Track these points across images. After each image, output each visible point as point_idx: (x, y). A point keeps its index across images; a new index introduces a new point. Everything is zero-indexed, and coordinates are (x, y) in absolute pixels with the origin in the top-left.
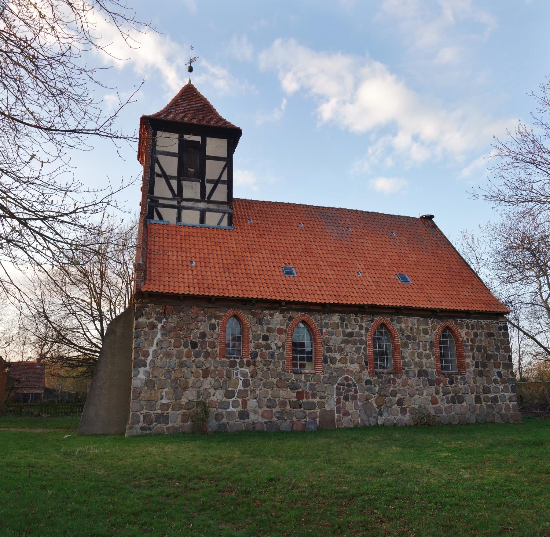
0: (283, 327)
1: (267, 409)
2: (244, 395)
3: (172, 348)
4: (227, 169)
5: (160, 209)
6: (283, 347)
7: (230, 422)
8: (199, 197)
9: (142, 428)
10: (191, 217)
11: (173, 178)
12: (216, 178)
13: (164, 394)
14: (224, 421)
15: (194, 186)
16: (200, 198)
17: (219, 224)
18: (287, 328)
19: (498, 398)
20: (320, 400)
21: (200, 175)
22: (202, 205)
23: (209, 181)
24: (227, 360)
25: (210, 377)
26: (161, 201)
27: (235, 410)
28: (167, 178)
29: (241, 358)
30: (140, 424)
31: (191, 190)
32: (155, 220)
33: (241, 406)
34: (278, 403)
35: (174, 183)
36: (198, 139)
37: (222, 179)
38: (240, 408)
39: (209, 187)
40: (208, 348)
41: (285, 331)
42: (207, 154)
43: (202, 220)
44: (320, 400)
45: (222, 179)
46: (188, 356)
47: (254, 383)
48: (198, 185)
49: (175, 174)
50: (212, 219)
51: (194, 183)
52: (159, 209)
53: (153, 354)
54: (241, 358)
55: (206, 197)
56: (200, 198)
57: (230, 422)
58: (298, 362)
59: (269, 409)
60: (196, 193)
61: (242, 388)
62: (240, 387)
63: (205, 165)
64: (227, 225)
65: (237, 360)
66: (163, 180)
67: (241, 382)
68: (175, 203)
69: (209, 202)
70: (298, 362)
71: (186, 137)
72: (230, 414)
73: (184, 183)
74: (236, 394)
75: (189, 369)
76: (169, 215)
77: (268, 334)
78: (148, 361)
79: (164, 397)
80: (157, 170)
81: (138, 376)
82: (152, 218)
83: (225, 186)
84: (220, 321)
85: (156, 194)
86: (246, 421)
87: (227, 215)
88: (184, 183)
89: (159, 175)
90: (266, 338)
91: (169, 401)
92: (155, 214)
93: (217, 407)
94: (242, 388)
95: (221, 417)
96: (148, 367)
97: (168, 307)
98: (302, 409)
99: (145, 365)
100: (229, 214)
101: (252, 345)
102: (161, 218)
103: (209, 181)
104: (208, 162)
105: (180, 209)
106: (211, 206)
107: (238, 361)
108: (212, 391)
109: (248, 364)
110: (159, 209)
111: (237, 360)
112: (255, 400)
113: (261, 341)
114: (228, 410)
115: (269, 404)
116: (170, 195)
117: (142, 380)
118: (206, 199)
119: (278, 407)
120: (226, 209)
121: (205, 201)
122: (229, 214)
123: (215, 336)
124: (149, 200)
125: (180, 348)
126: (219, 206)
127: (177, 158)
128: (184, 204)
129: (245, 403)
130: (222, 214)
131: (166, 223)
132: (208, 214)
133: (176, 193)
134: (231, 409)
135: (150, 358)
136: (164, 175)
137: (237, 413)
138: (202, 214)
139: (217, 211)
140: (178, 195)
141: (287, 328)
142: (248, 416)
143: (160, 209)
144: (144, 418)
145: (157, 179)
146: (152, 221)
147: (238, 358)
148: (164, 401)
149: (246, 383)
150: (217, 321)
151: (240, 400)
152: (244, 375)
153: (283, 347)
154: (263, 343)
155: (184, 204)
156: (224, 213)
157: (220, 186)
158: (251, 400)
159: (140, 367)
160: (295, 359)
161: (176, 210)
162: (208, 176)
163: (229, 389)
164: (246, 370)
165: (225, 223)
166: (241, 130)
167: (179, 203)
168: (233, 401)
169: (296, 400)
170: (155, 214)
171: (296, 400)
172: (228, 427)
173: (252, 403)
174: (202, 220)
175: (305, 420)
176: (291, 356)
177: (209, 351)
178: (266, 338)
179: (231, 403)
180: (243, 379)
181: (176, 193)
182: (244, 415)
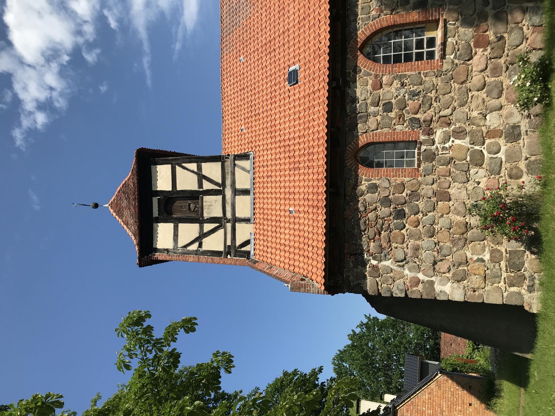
0: (370, 82)
1: (504, 96)
2: (480, 134)
3: (405, 245)
4: (184, 165)
5: (238, 243)
6: (400, 77)
7: (524, 155)
8: (220, 197)
9: (531, 289)
10: (243, 207)
11: (201, 228)
12: (196, 177)
13: (475, 258)
14: (522, 165)
15: (208, 204)
16: (221, 196)
17: (249, 172)
18: (371, 75)
19: (402, 219)
20: (491, 6)
21: (195, 196)
22: (228, 193)
23: (200, 185)
24: (423, 166)
25: (449, 190)
26: (229, 243)
27: (503, 149)
28: (203, 235)
29: (421, 143)
30: (523, 292)
31: (212, 206)
32: (251, 249)
33: (497, 140)
34: (493, 79)
35: (208, 227)
36: (155, 200)
37: (196, 170)
38: (501, 141)
39: (207, 186)
40: (404, 194)
41: (376, 76)
42: (170, 189)
43: (246, 192)
44: (491, 6)
45: (196, 170)
46: (417, 224)
47: (458, 120)
48: (206, 198)
49: (197, 226)
50: (243, 180)
51: (204, 204)
52: (238, 244)
53: (414, 272)
54: (421, 143)
55: (219, 188)
56: (221, 196)
57: (524, 155)
58: (425, 50)
59: (504, 92)
60: (216, 201)
61: (468, 139)
62: (465, 143)
63: (182, 191)
64: (249, 161)
65: (422, 150)
66: (205, 241)
67: (457, 142)
68: (229, 226)
69: (223, 184)
70: (425, 50)
71: (156, 213)
72: (510, 157)
73: (206, 215)
74: (477, 148)
75: (436, 221)
76: (244, 232)
77: (381, 104)
78: (426, 279)
79: (480, 257)
80: (194, 247)
81: (448, 293)
82: (248, 253)
83: (204, 165)
84: (364, 178)
85: (221, 248)
86: (523, 129)
87: (236, 162)
88: (206, 215)
89: (200, 245)
90: (388, 107)
91: (487, 249)
92: (243, 249)
93: (497, 177)
94: (468, 139)
95: (514, 171)
96: (433, 279)
97: (346, 251)
98: (506, 35)
99: (432, 283)
100: (235, 159)
101: (399, 128)
102: (247, 243)
103: (200, 185)
104: (179, 188)
105: (235, 220)
106: (228, 182)
107: (423, 148)
108: (470, 186)
109: (430, 132)
110: (238, 244)
111: (422, 150)
112: (487, 117)
113: (392, 115)
114: (504, 160)
115: (495, 93)
116: (221, 232)
117: (453, 288)
118: (221, 188)
119: (501, 78)
120: (229, 163)
121: (224, 188)
122: (235, 159)
123: (386, 184)
124: (229, 256)
125: (405, 234)
126: (228, 173)
127: (179, 224)
128: (229, 215)
129: (493, 133)
130: (236, 168)
131: (253, 237)
132: (238, 186)
133: (218, 224)
134: (501, 155)
135: (421, 276)
136: (199, 239)
137: (509, 145)
138: (237, 192)
139: (233, 174)
140: (219, 222)
141: (371, 75)
142: (516, 127)
143: (238, 243)
144: (513, 285)
145: (205, 247)
146: (252, 253)
147: (419, 149)
148: (487, 257)
149: (459, 134)
150: (363, 182)
151: (487, 141)
152: (446, 139)
153: (400, 77)
154: (395, 111)
155: (229, 215)
156: (235, 165)
157: (204, 172)
158: (488, 123)
159: (434, 290)
160: (419, 57)
161: (238, 225)
162: (195, 187)
163: (468, 159)
164: (438, 135)
165: (246, 164)
166: (138, 150)
167: (229, 221)
168: (489, 153)
169: (489, 49)
170: (243, 249)
171: (489, 49)
172: (533, 158)
173: (493, 121)
174: (246, 192)
175: (525, 28)
176: (414, 63)
177: (409, 192)
178: (388, 107)
179: (491, 156)
180: (452, 139)
181: (218, 224)
182: (513, 134)
